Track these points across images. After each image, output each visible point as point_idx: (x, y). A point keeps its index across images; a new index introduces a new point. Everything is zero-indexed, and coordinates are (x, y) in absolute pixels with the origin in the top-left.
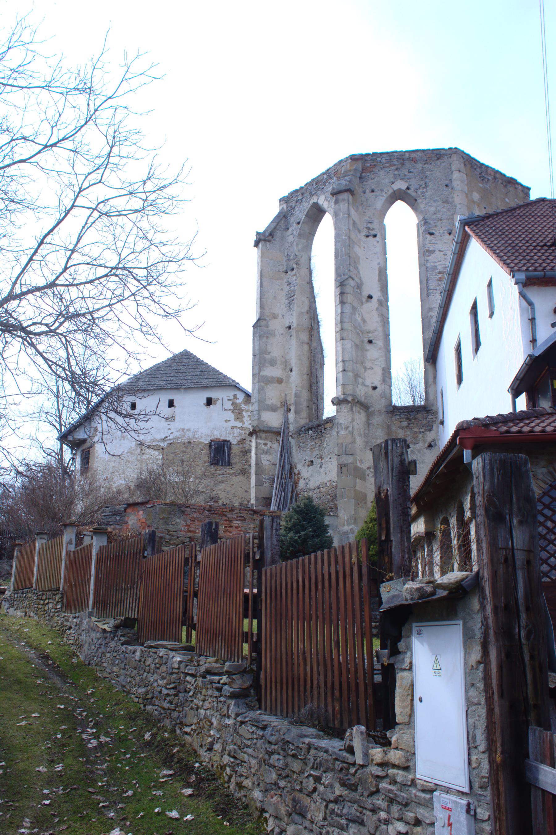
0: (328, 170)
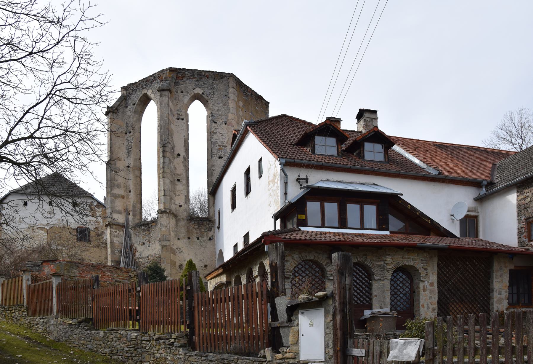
0: (154, 74)
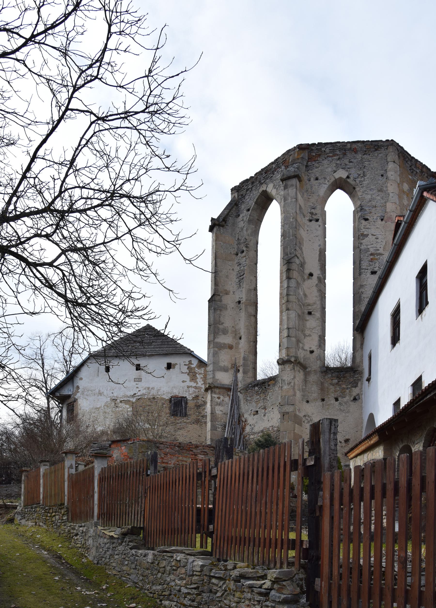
0: (276, 160)
